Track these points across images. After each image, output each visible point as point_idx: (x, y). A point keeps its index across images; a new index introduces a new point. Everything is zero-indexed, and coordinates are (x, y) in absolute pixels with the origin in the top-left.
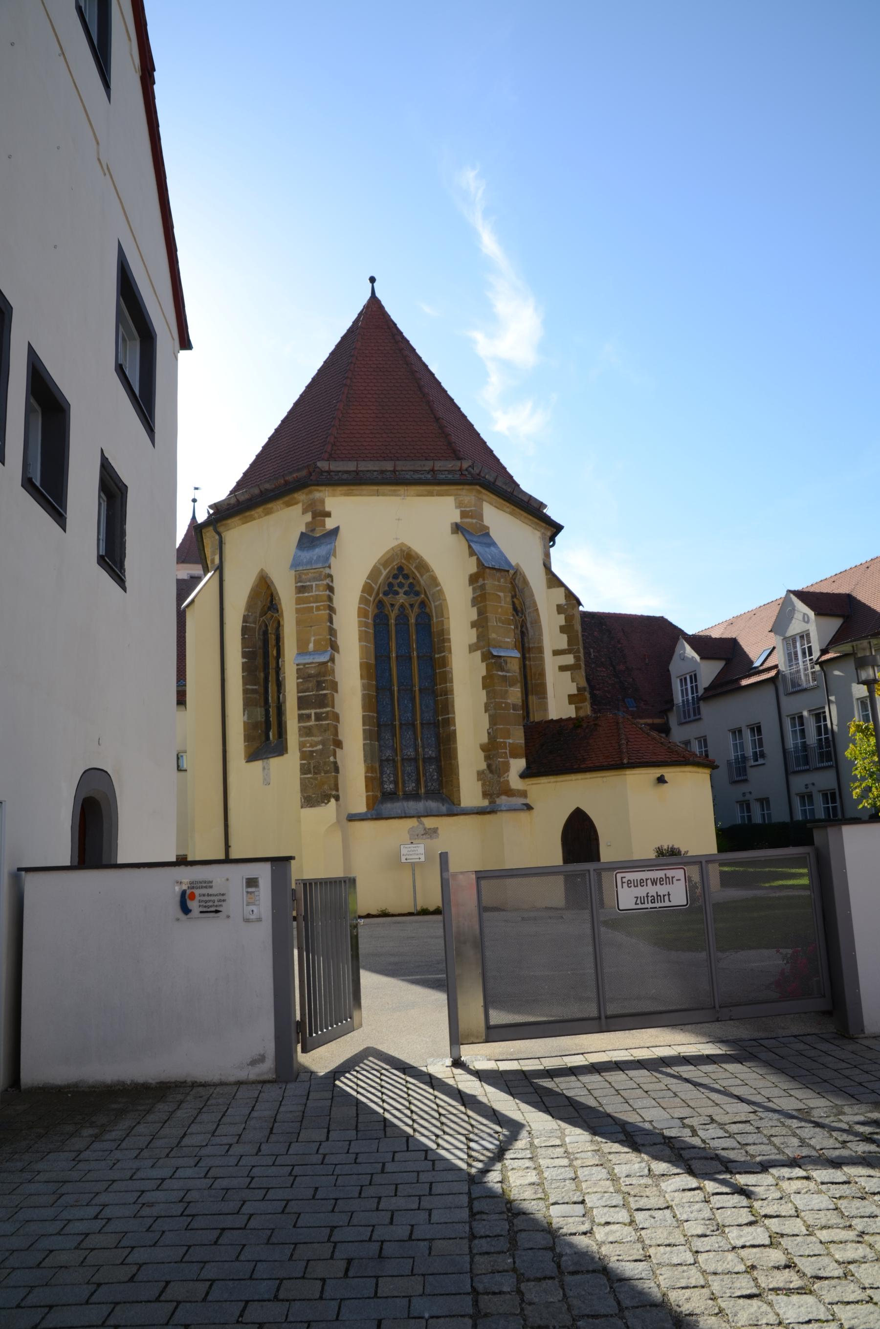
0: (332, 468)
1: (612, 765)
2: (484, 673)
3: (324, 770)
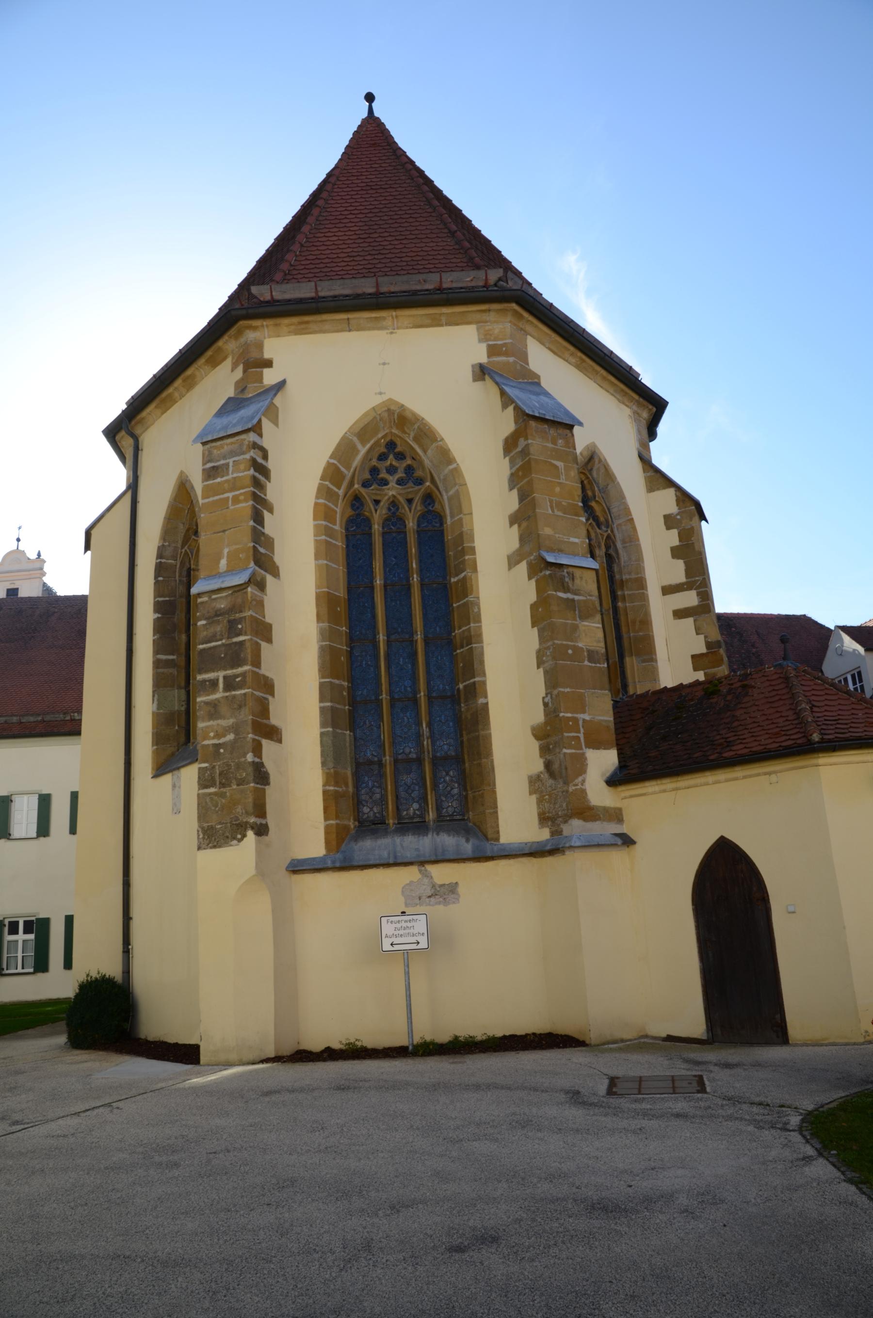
0: (277, 296)
1: (786, 748)
2: (533, 597)
3: (236, 778)
